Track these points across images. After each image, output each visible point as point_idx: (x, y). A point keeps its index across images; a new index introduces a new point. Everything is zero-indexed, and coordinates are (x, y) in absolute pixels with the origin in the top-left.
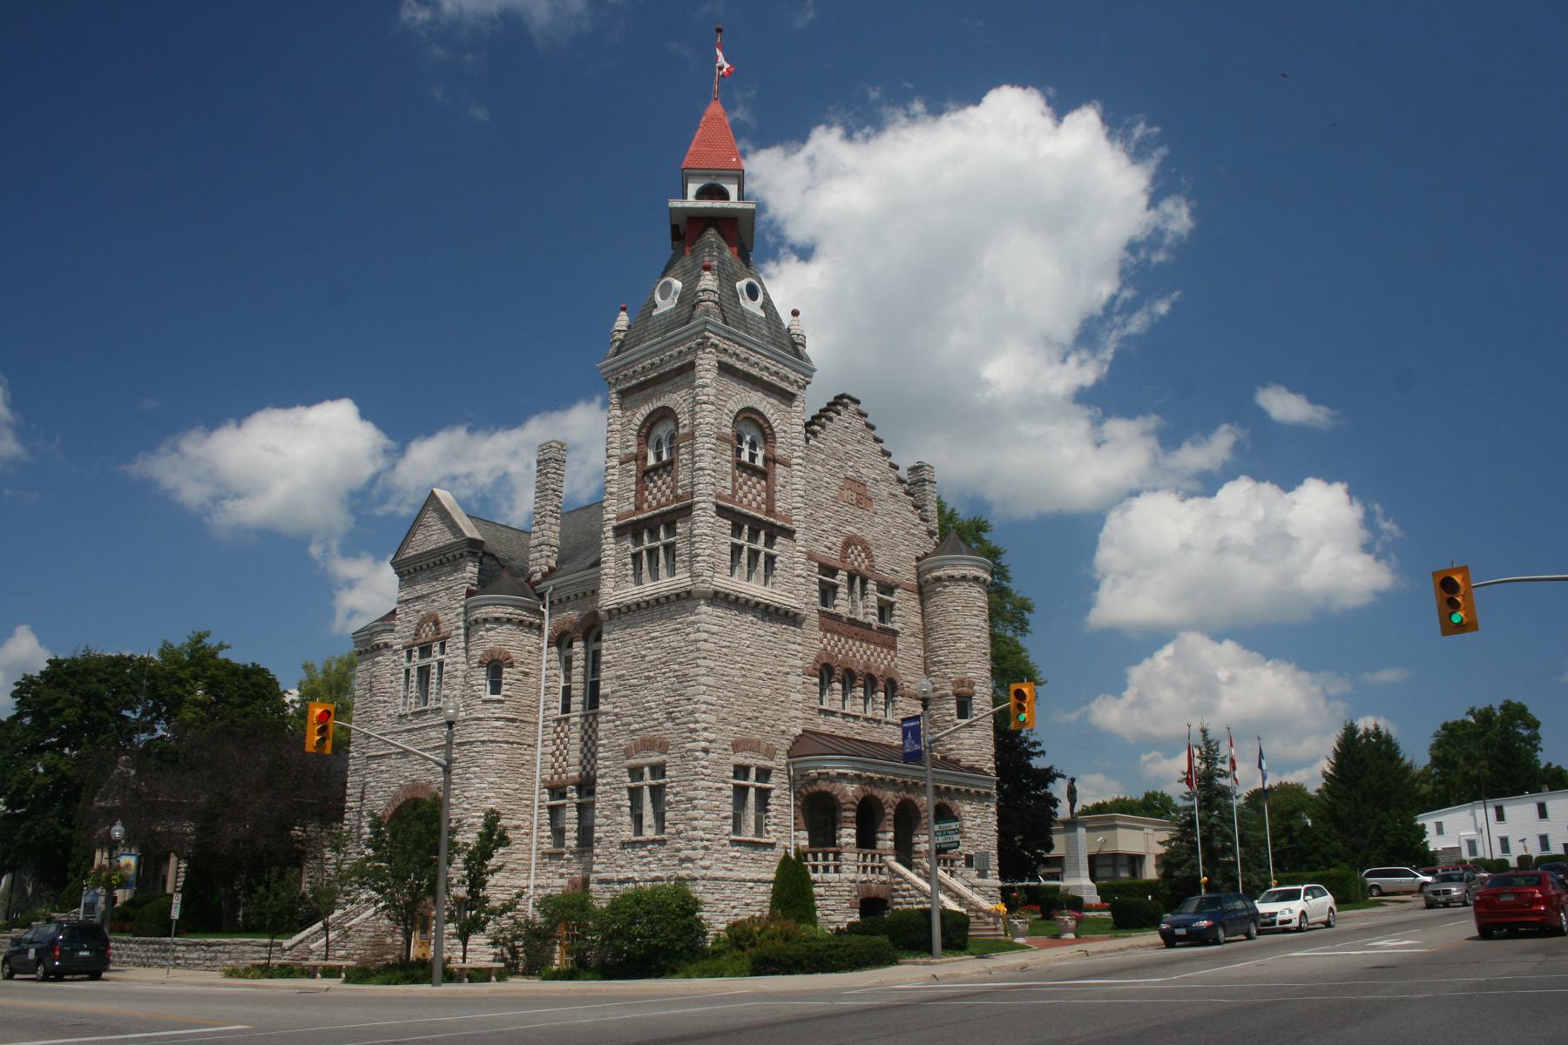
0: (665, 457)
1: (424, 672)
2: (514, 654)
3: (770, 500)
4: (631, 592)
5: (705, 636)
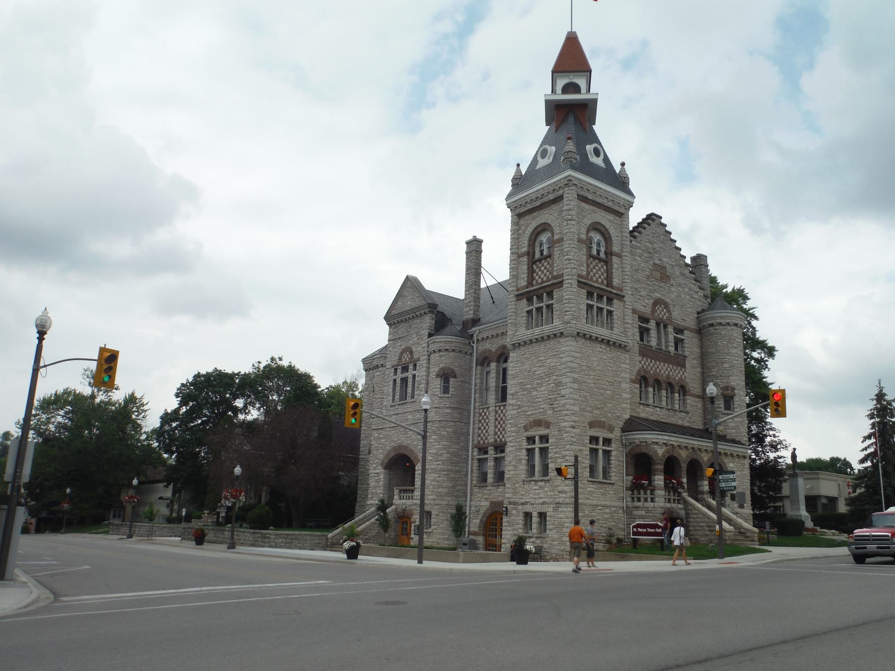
0: (545, 253)
1: (404, 380)
2: (456, 370)
3: (609, 278)
4: (524, 333)
5: (572, 359)
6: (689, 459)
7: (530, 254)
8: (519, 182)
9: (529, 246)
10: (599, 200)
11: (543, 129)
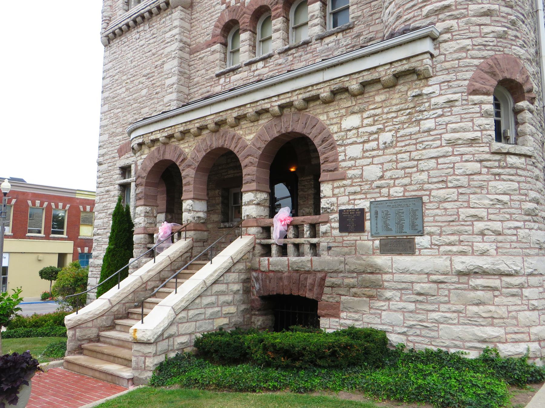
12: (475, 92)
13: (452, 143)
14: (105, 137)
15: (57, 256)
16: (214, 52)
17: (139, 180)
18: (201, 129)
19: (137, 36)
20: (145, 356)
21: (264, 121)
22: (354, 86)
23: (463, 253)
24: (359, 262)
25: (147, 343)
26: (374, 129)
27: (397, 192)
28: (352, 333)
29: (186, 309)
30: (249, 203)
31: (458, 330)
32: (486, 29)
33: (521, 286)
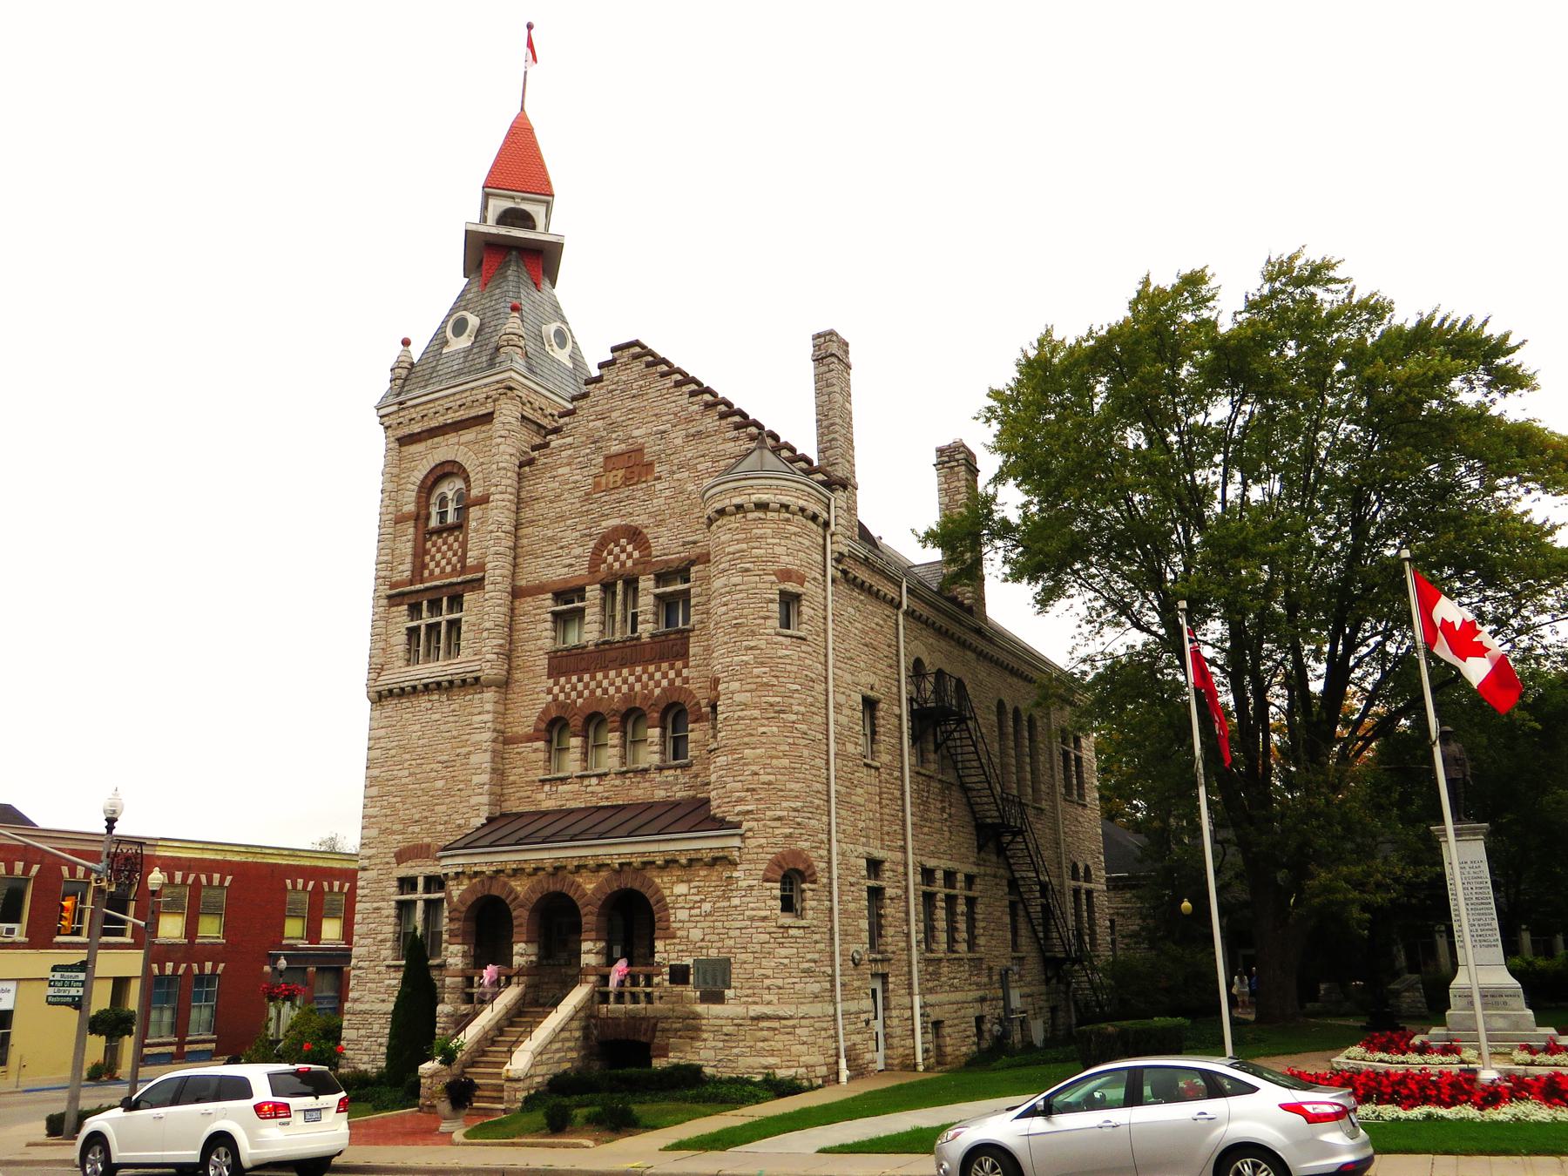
6: (535, 897)
7: (420, 517)
8: (406, 376)
9: (418, 503)
10: (439, 421)
11: (457, 281)
12: (767, 880)
13: (752, 919)
14: (374, 832)
15: (110, 983)
16: (536, 750)
17: (456, 915)
18: (536, 870)
19: (429, 705)
20: (516, 1090)
21: (604, 874)
22: (683, 861)
23: (755, 1003)
24: (1182, 621)
25: (518, 1080)
26: (697, 898)
27: (713, 953)
28: (677, 1067)
29: (541, 1054)
30: (589, 952)
31: (750, 1061)
32: (777, 832)
33: (794, 1027)
